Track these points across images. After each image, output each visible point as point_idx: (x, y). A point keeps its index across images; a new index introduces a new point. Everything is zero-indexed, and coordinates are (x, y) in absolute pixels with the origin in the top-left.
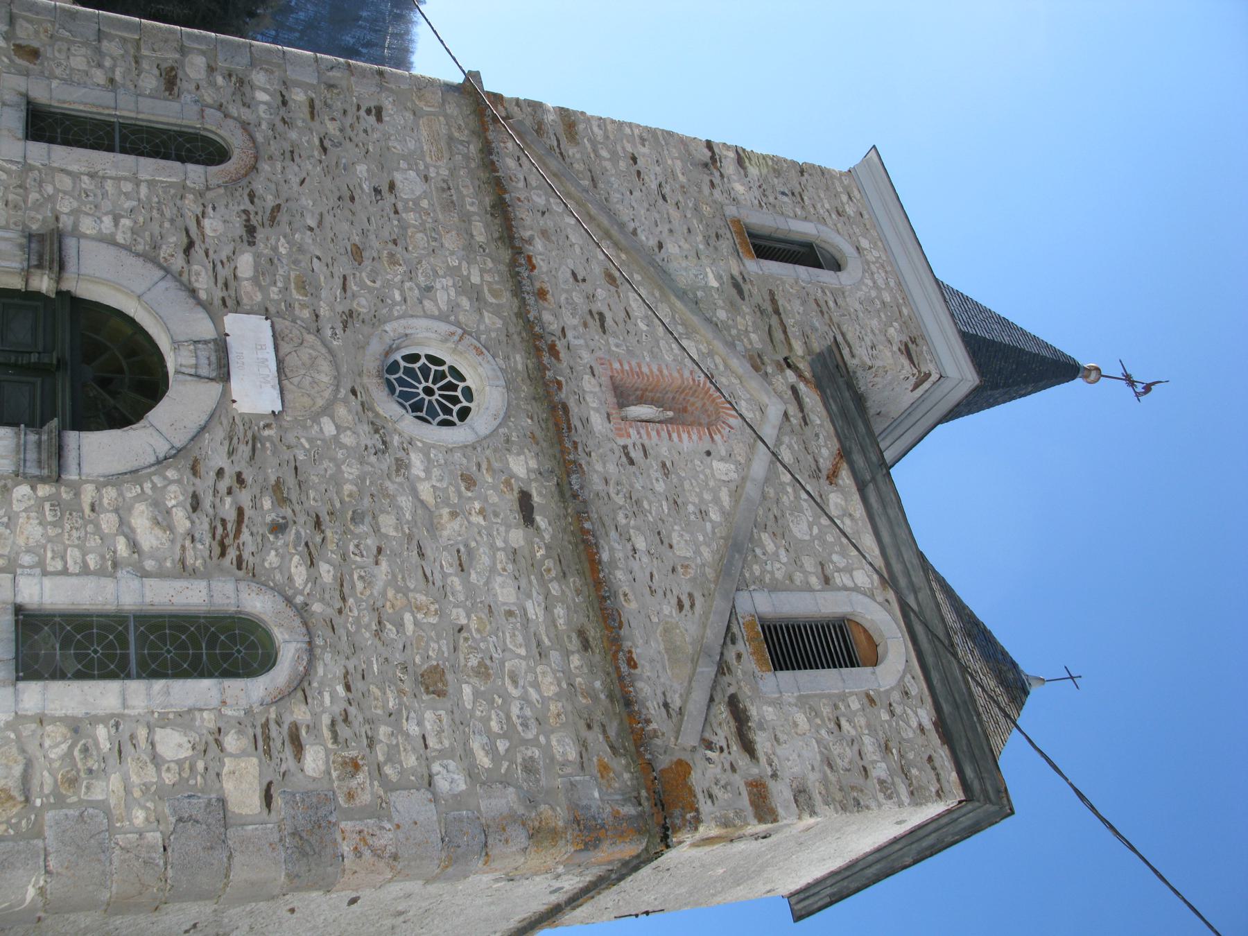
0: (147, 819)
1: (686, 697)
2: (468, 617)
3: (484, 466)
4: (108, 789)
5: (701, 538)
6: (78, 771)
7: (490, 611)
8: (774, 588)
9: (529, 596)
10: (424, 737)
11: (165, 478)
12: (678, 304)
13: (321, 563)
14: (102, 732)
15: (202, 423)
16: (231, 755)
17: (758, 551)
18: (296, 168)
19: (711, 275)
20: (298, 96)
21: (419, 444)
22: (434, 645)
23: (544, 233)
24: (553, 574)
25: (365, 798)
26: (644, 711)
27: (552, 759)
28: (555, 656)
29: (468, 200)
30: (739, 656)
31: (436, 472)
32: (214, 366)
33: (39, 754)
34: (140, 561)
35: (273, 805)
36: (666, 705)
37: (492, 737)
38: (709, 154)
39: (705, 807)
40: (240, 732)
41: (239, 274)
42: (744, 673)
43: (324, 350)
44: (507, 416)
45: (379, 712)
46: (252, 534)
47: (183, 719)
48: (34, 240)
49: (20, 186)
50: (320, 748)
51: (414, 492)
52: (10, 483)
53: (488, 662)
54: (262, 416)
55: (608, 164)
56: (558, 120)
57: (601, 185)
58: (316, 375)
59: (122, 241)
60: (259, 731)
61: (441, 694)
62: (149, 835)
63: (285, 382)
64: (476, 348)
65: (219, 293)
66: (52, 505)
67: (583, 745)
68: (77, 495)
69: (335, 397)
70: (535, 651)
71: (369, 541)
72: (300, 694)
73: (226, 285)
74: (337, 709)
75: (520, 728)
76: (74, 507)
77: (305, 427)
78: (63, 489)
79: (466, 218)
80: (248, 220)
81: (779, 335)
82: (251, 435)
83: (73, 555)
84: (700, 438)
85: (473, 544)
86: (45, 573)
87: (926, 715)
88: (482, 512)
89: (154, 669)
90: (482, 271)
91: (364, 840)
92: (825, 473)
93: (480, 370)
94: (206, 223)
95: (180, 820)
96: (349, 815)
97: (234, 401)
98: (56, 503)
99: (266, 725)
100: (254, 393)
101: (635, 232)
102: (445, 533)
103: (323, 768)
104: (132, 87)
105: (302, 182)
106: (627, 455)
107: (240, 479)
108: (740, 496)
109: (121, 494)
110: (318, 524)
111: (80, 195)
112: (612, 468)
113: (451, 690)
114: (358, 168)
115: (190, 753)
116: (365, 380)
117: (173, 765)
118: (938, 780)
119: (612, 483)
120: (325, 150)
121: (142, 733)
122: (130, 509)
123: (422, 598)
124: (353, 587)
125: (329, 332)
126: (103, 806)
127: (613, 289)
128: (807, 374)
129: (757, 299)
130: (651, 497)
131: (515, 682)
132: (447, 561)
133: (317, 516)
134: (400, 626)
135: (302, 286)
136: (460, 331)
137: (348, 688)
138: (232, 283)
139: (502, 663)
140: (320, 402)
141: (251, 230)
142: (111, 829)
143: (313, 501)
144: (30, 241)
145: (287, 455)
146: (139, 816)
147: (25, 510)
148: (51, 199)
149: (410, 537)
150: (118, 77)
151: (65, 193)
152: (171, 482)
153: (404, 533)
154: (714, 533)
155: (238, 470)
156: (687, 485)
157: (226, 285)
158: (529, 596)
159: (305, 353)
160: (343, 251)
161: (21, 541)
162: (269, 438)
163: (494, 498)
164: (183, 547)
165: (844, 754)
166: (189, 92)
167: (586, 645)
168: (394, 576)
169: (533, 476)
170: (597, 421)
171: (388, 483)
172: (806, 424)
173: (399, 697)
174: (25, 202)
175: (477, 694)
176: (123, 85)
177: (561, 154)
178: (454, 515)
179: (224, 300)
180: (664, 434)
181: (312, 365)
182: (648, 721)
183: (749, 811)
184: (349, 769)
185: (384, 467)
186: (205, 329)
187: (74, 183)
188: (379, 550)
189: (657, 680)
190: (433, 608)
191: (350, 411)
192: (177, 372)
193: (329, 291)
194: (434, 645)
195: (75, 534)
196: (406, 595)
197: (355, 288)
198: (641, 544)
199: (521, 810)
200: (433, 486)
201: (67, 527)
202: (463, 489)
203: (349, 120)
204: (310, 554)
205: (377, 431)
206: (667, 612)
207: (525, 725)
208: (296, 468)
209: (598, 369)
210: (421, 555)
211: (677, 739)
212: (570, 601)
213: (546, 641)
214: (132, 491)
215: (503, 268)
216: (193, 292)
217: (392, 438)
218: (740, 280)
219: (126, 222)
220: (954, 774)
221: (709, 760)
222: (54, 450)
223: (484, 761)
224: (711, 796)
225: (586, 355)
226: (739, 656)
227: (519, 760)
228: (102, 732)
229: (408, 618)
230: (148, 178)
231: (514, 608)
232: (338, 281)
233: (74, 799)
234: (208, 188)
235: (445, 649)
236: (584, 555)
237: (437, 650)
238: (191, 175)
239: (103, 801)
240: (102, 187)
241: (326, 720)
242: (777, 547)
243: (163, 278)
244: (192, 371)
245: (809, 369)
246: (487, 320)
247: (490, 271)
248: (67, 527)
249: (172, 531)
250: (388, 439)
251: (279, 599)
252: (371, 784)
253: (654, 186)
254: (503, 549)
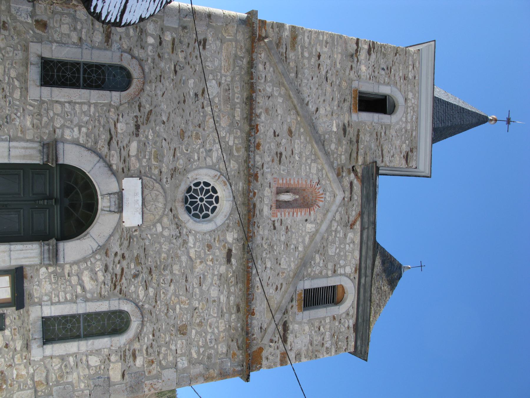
0: (85, 386)
2: (199, 304)
3: (217, 239)
4: (73, 378)
5: (292, 259)
6: (63, 373)
7: (207, 301)
9: (222, 293)
10: (176, 350)
11: (96, 259)
12: (315, 146)
13: (150, 288)
14: (71, 359)
15: (111, 233)
16: (113, 362)
17: (312, 262)
18: (161, 86)
19: (335, 125)
20: (168, 37)
21: (193, 232)
22: (185, 316)
23: (267, 111)
24: (233, 283)
25: (154, 372)
26: (253, 331)
27: (218, 353)
28: (227, 315)
29: (237, 95)
30: (292, 307)
31: (198, 244)
32: (117, 206)
33: (51, 368)
34: (86, 294)
35: (125, 378)
36: (261, 328)
37: (199, 347)
38: (355, 47)
40: (116, 355)
41: (131, 154)
42: (292, 313)
43: (161, 191)
44: (230, 214)
45: (163, 342)
46: (126, 279)
47: (97, 352)
48: (45, 146)
49: (39, 115)
50: (142, 357)
51: (188, 253)
52: (38, 267)
53: (203, 321)
54: (134, 227)
55: (306, 61)
56: (289, 36)
57: (299, 76)
58: (157, 204)
59: (82, 142)
60: (122, 353)
61: (184, 334)
62: (85, 391)
63: (145, 209)
64: (224, 182)
65: (121, 165)
66: (54, 276)
67: (229, 347)
68: (63, 269)
69: (164, 214)
70: (220, 314)
71: (168, 277)
72: (137, 339)
73: (125, 161)
74: (149, 343)
75: (209, 343)
76: (62, 276)
77: (150, 229)
78: (58, 268)
79: (233, 109)
80: (137, 122)
81: (354, 155)
82: (129, 236)
83: (62, 294)
84: (305, 214)
85: (206, 274)
86: (52, 304)
88: (212, 260)
89: (89, 335)
90: (235, 138)
91: (152, 386)
92: (350, 223)
93: (224, 192)
94: (119, 125)
95: (95, 386)
96: (148, 379)
97: (124, 222)
98: (55, 273)
99: (125, 351)
100: (132, 217)
101: (307, 104)
102: (197, 270)
103: (142, 364)
104: (90, 42)
105: (163, 94)
106: (274, 225)
107: (123, 257)
108: (313, 240)
109: (79, 267)
110: (150, 272)
111: (64, 116)
112: (266, 232)
113: (188, 332)
114: (190, 82)
115: (99, 363)
116: (177, 204)
117: (94, 368)
118: (347, 346)
119: (264, 239)
120: (176, 72)
121: (84, 358)
122: (82, 273)
123: (184, 298)
124: (160, 296)
125: (165, 180)
126: (71, 383)
127: (289, 138)
128: (359, 175)
129: (351, 135)
130: (278, 244)
131: (210, 327)
132: (195, 282)
133: (151, 269)
135: (156, 158)
136: (219, 174)
137: (153, 335)
138: (127, 159)
139: (208, 320)
140: (157, 217)
141: (137, 127)
142: (74, 391)
143: (150, 262)
144: (43, 148)
145: (142, 243)
146: (82, 385)
147: (44, 278)
148: (52, 120)
149: (183, 274)
150: (84, 37)
151: (58, 115)
152: (98, 260)
153: (181, 272)
154: (298, 256)
155: (123, 252)
156: (294, 236)
157: (125, 161)
158: (222, 293)
159: (154, 193)
160: (176, 134)
161: (43, 291)
162: (136, 236)
163: (217, 253)
164: (101, 288)
166: (117, 43)
167: (238, 310)
168: (175, 291)
169: (234, 241)
170: (266, 211)
171: (179, 251)
172: (351, 200)
173: (170, 337)
174: (41, 123)
175: (197, 332)
176: (86, 41)
177: (286, 57)
178: (201, 262)
179: (123, 169)
180: (291, 214)
181: (156, 200)
182: (253, 335)
183: (279, 362)
184: (151, 363)
185: (178, 244)
186: (114, 187)
187: (62, 109)
188: (172, 280)
189: (262, 317)
190: (187, 302)
191: (168, 220)
192: (102, 210)
193: (168, 158)
194: (185, 316)
195: (62, 286)
196: (178, 298)
197: (179, 155)
198: (269, 265)
199: (203, 372)
200: (196, 251)
201: (60, 284)
202: (207, 251)
203: (190, 50)
204: (146, 285)
205: (178, 228)
206: (271, 292)
207: (211, 342)
208: (145, 249)
209: (273, 184)
210: (186, 281)
211: (262, 340)
212: (237, 294)
213: (225, 310)
215: (244, 135)
216: (110, 166)
217: (183, 230)
218: (347, 125)
219: (84, 130)
220: (353, 343)
221: (270, 346)
222: (55, 254)
223: (195, 356)
224: (267, 359)
225: (269, 176)
226: (292, 307)
227: (206, 355)
228: (71, 359)
229: (178, 306)
230: (94, 102)
231: (216, 299)
232: (172, 152)
233: (62, 382)
234: (121, 104)
235: (189, 317)
236: (246, 278)
237: (186, 318)
238: (114, 98)
239: (71, 382)
240: (74, 109)
241: (145, 347)
242: (320, 260)
243: (98, 162)
244: (108, 209)
245: (361, 172)
246: (232, 166)
247: (238, 137)
248: (60, 284)
249: (97, 281)
250: (181, 231)
251: (134, 305)
252: (157, 368)
253: (324, 73)
254: (217, 275)
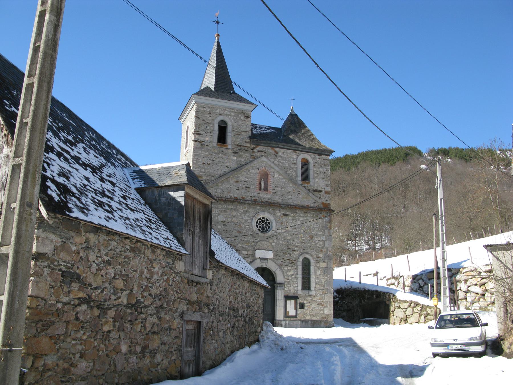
1: (313, 199)
8: (297, 175)
23: (229, 193)
39: (328, 202)
47: (315, 271)
79: (228, 209)
81: (246, 148)
82: (276, 256)
83: (295, 283)
87: (317, 156)
96: (327, 252)
107: (283, 259)
110: (289, 249)
112: (277, 197)
126: (325, 282)
134: (303, 240)
135: (248, 243)
143: (286, 248)
145: (279, 251)
159: (261, 245)
165: (322, 175)
167: (306, 212)
170: (269, 196)
198: (290, 197)
214: (285, 274)
223: (321, 233)
225: (255, 194)
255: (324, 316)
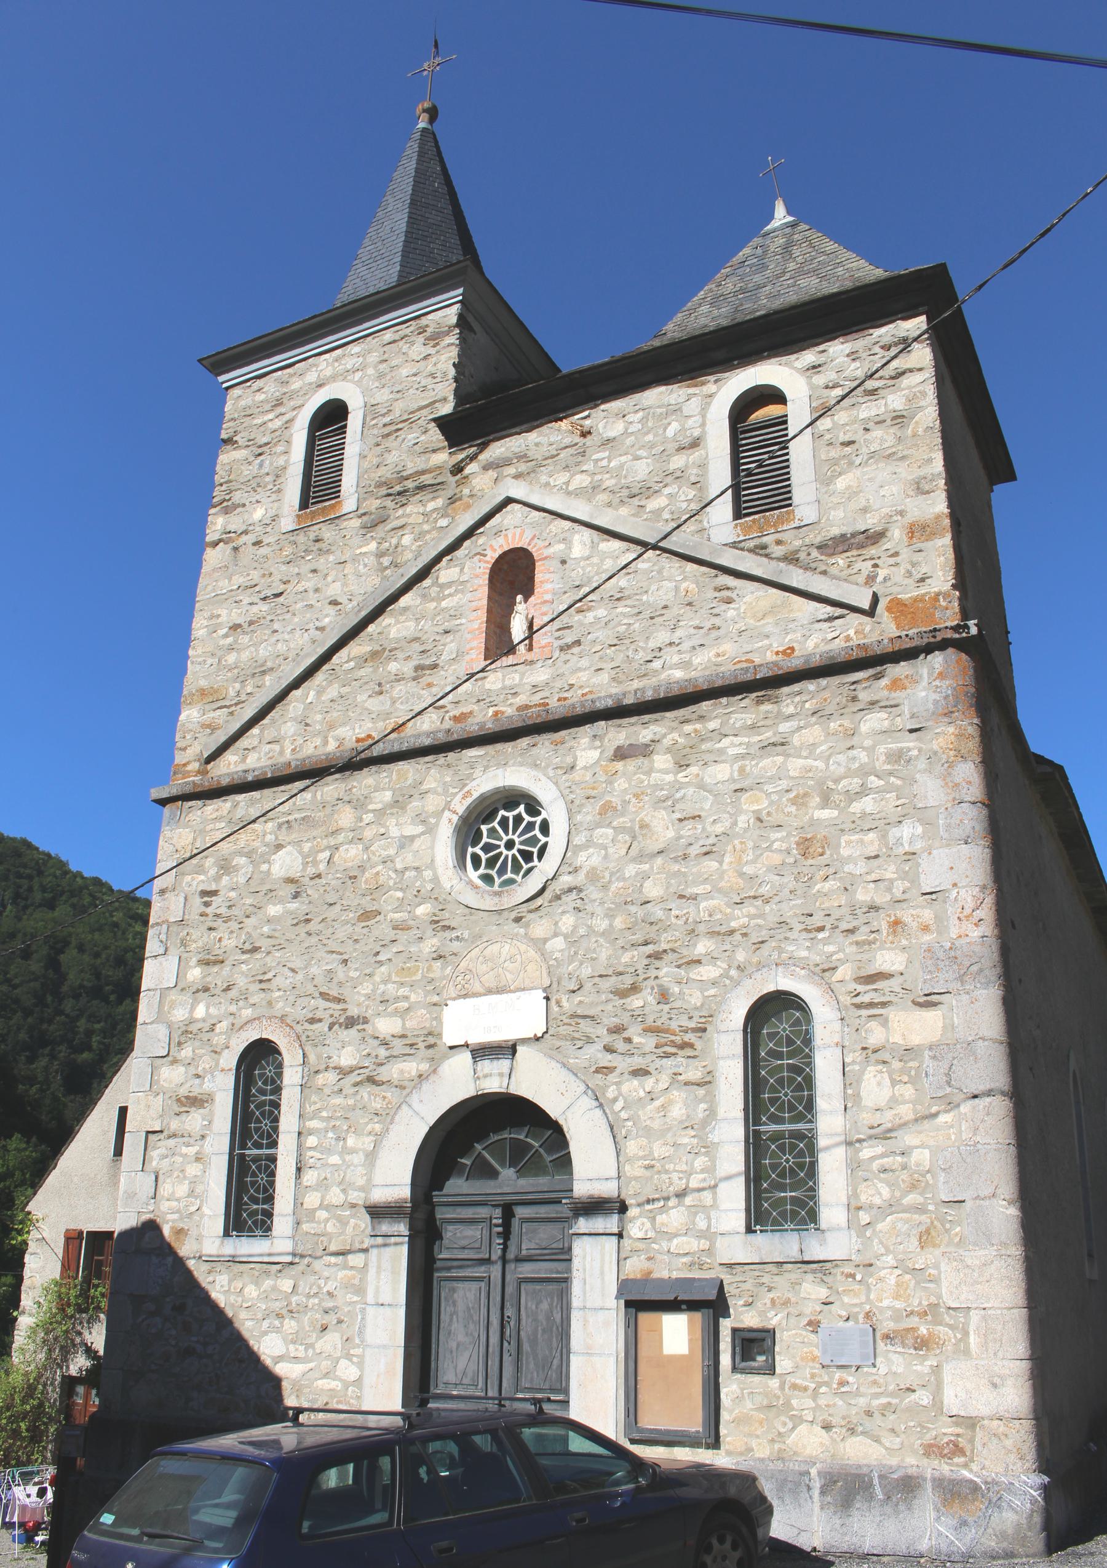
255: (947, 1430)
